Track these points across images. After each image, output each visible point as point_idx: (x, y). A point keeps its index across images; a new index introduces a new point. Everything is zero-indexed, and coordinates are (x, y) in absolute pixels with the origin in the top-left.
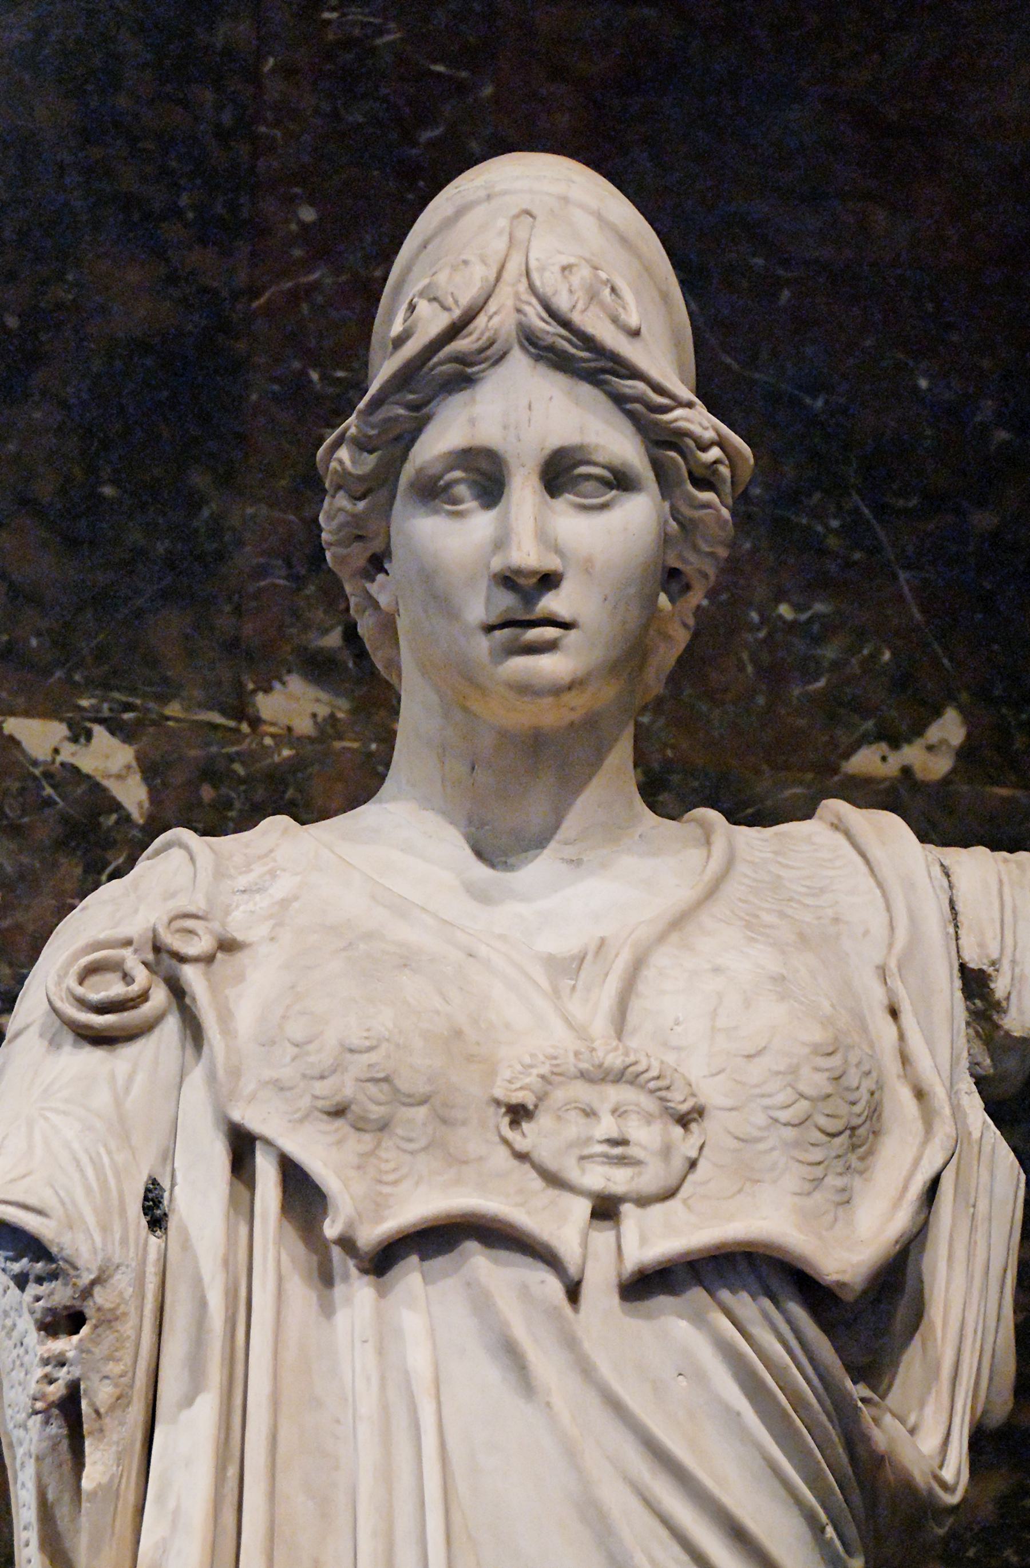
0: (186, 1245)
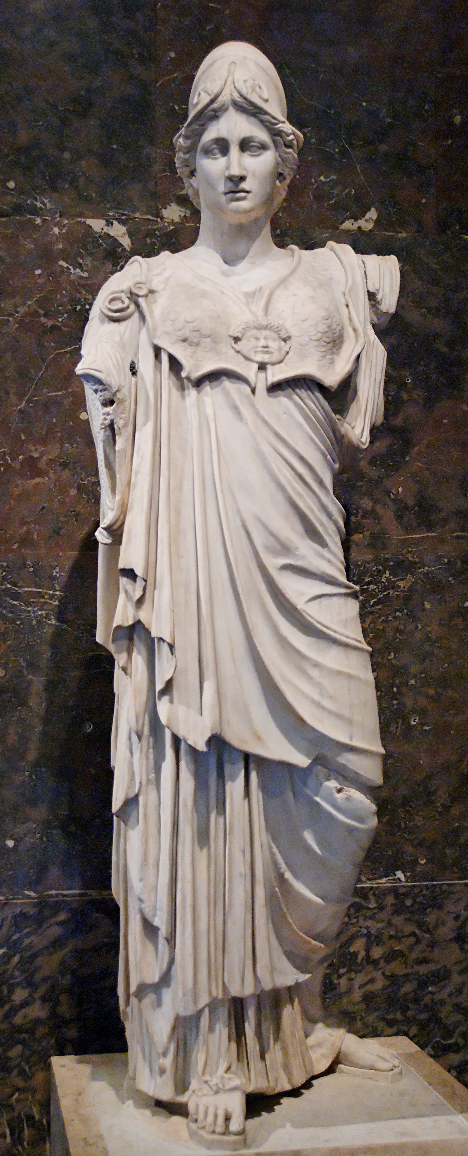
0: (143, 379)
